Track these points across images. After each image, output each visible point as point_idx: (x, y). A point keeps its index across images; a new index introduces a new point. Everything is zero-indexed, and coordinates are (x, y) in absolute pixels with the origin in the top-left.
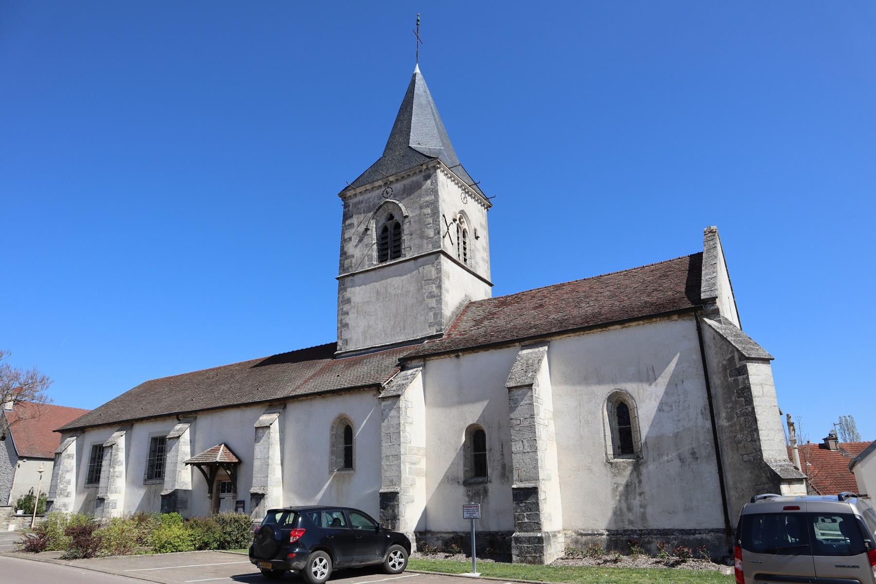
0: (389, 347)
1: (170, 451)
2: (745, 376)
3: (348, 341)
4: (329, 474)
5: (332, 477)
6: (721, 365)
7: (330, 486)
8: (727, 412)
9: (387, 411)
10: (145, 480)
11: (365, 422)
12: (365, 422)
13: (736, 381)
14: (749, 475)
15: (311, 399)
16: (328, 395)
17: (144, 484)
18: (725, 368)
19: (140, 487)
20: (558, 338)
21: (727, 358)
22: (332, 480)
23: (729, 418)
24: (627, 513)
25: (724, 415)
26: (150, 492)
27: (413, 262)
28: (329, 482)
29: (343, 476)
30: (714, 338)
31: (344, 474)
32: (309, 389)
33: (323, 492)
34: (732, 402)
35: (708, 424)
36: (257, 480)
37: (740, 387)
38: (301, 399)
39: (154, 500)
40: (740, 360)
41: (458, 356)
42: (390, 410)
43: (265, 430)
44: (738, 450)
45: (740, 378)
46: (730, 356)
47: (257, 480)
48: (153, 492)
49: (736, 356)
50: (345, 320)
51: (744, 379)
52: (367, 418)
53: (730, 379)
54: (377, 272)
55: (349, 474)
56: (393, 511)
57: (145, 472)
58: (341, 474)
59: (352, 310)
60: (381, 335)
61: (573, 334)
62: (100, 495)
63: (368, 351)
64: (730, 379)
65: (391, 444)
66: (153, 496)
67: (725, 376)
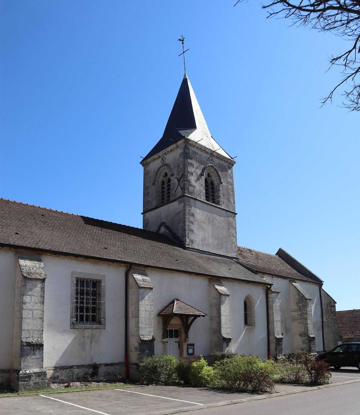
0: (212, 254)
1: (142, 299)
2: (334, 308)
3: (193, 241)
4: (244, 327)
5: (245, 330)
6: (326, 303)
7: (245, 334)
8: (326, 317)
9: (275, 298)
10: (73, 324)
11: (259, 301)
12: (259, 301)
13: (331, 309)
14: (332, 336)
15: (233, 282)
16: (48, 254)
17: (71, 328)
18: (327, 304)
19: (64, 331)
20: (267, 275)
21: (329, 301)
22: (246, 330)
23: (327, 319)
24: (199, 363)
25: (325, 318)
26: (84, 337)
27: (225, 211)
28: (244, 332)
29: (250, 329)
30: (324, 294)
31: (251, 328)
32: (27, 242)
33: (242, 337)
34: (329, 314)
35: (321, 320)
36: (224, 330)
37: (333, 311)
38: (230, 280)
39: (91, 345)
40: (333, 303)
41: (272, 277)
42: (276, 298)
43: (226, 297)
44: (329, 329)
45: (333, 308)
46: (330, 301)
47: (224, 330)
48: (88, 337)
49: (332, 302)
50: (191, 226)
51: (334, 309)
52: (259, 300)
53: (329, 308)
54: (208, 206)
55: (253, 328)
56: (282, 347)
57: (72, 314)
58: (249, 328)
59: (196, 222)
60: (211, 246)
61: (300, 281)
62: (27, 337)
63: (205, 253)
64: (329, 308)
65: (277, 315)
66: (90, 342)
67: (327, 307)
